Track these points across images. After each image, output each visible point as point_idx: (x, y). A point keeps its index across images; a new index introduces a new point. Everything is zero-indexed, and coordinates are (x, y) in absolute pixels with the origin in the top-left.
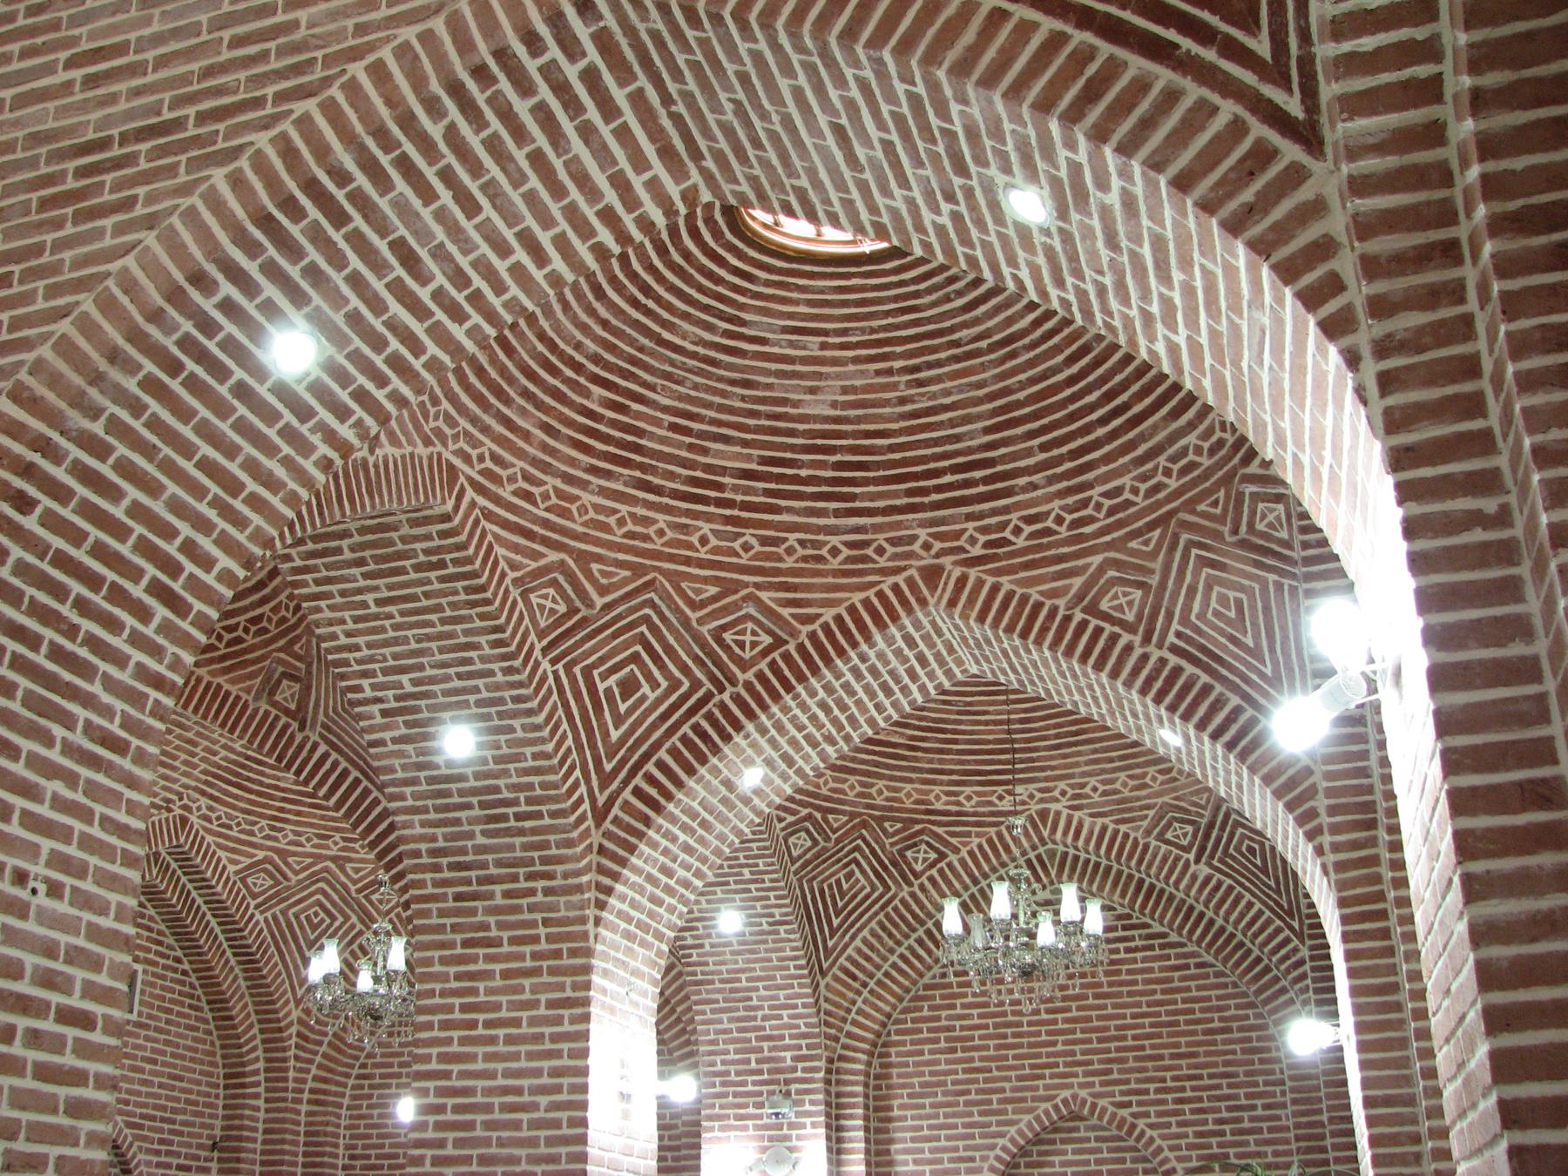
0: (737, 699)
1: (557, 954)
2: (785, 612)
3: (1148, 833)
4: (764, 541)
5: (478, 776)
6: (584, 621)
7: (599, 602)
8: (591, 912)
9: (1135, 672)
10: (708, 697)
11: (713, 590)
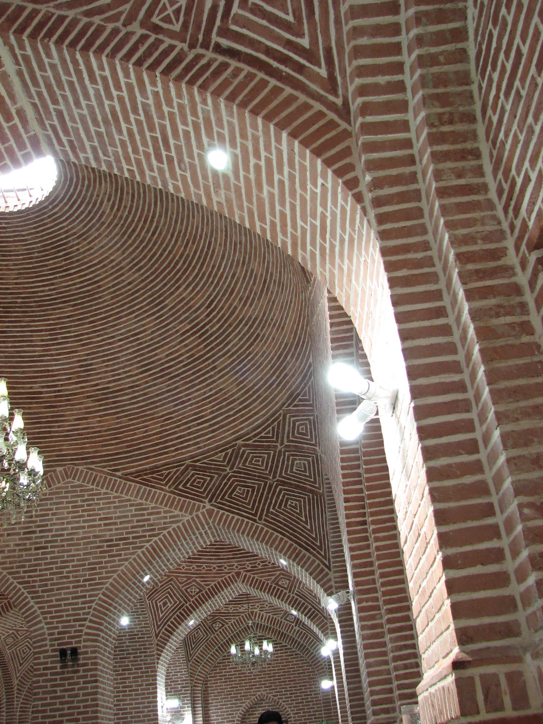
0: (190, 605)
1: (148, 672)
2: (202, 583)
3: (282, 618)
4: (198, 566)
5: (129, 629)
6: (156, 590)
7: (160, 585)
8: (156, 661)
9: (287, 599)
10: (184, 605)
11: (185, 579)
